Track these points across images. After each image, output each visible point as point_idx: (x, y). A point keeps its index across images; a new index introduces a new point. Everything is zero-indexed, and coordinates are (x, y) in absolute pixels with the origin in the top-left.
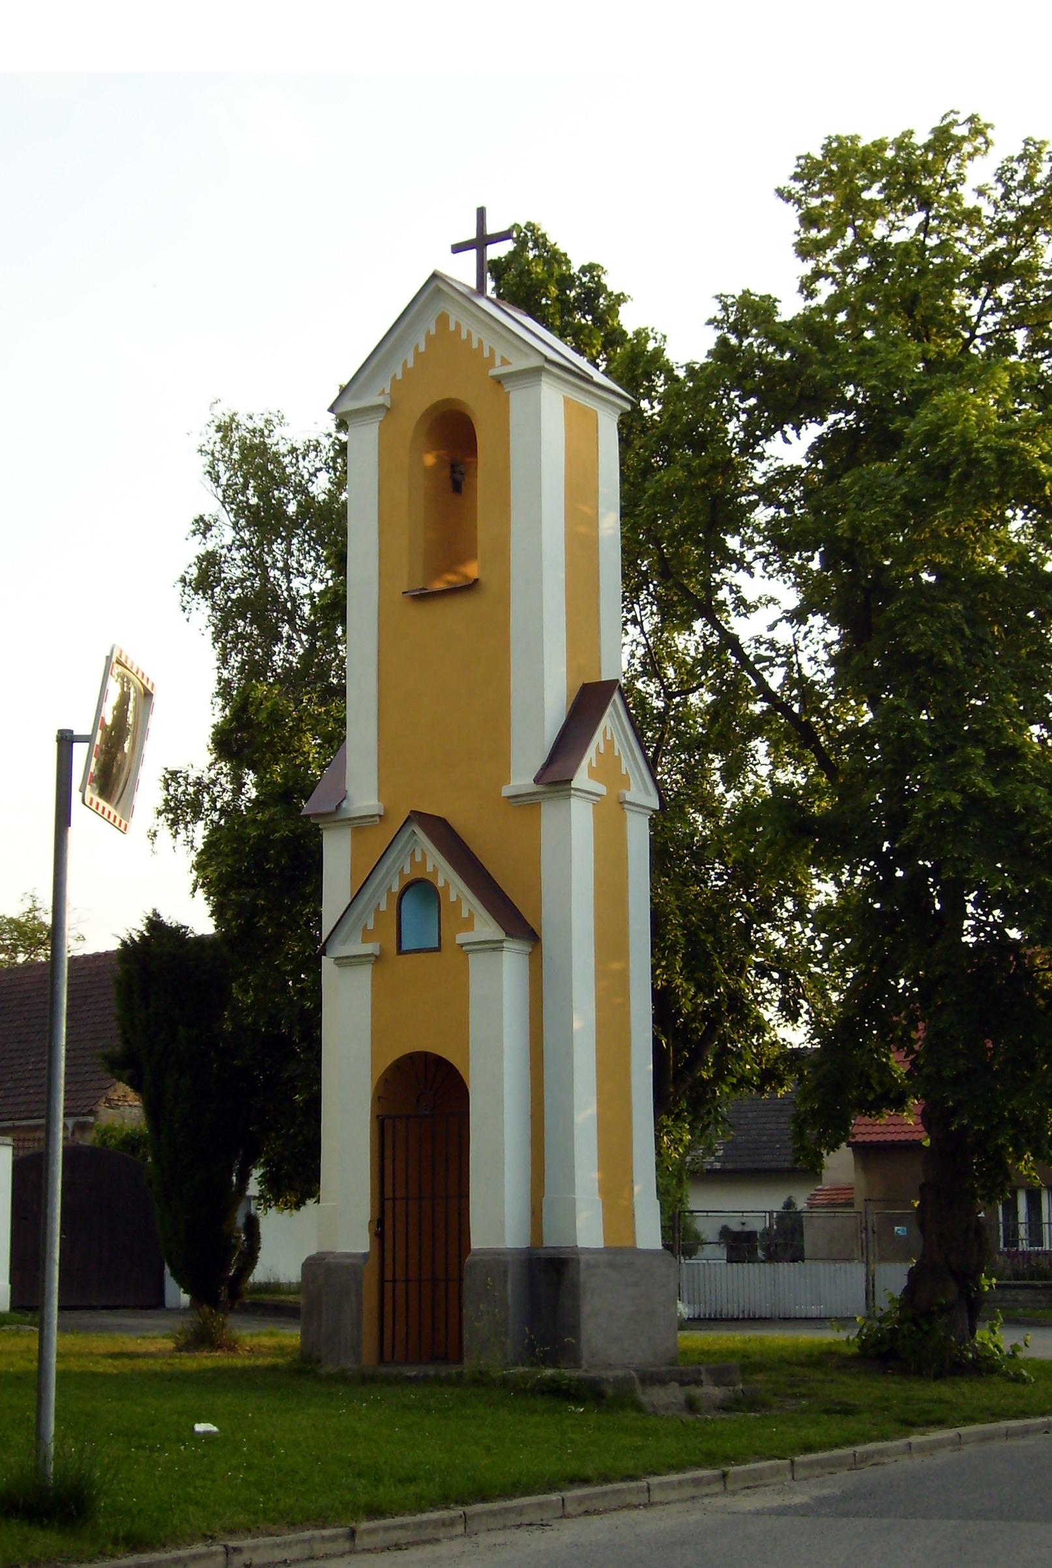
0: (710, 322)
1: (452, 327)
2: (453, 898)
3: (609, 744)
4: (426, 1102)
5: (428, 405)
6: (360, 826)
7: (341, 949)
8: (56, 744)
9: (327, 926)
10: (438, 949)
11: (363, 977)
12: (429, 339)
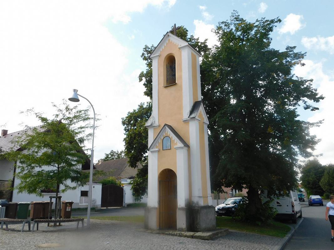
0: (217, 26)
1: (171, 41)
2: (173, 139)
3: (201, 112)
4: (168, 178)
5: (167, 54)
7: (151, 150)
10: (170, 149)
11: (156, 155)
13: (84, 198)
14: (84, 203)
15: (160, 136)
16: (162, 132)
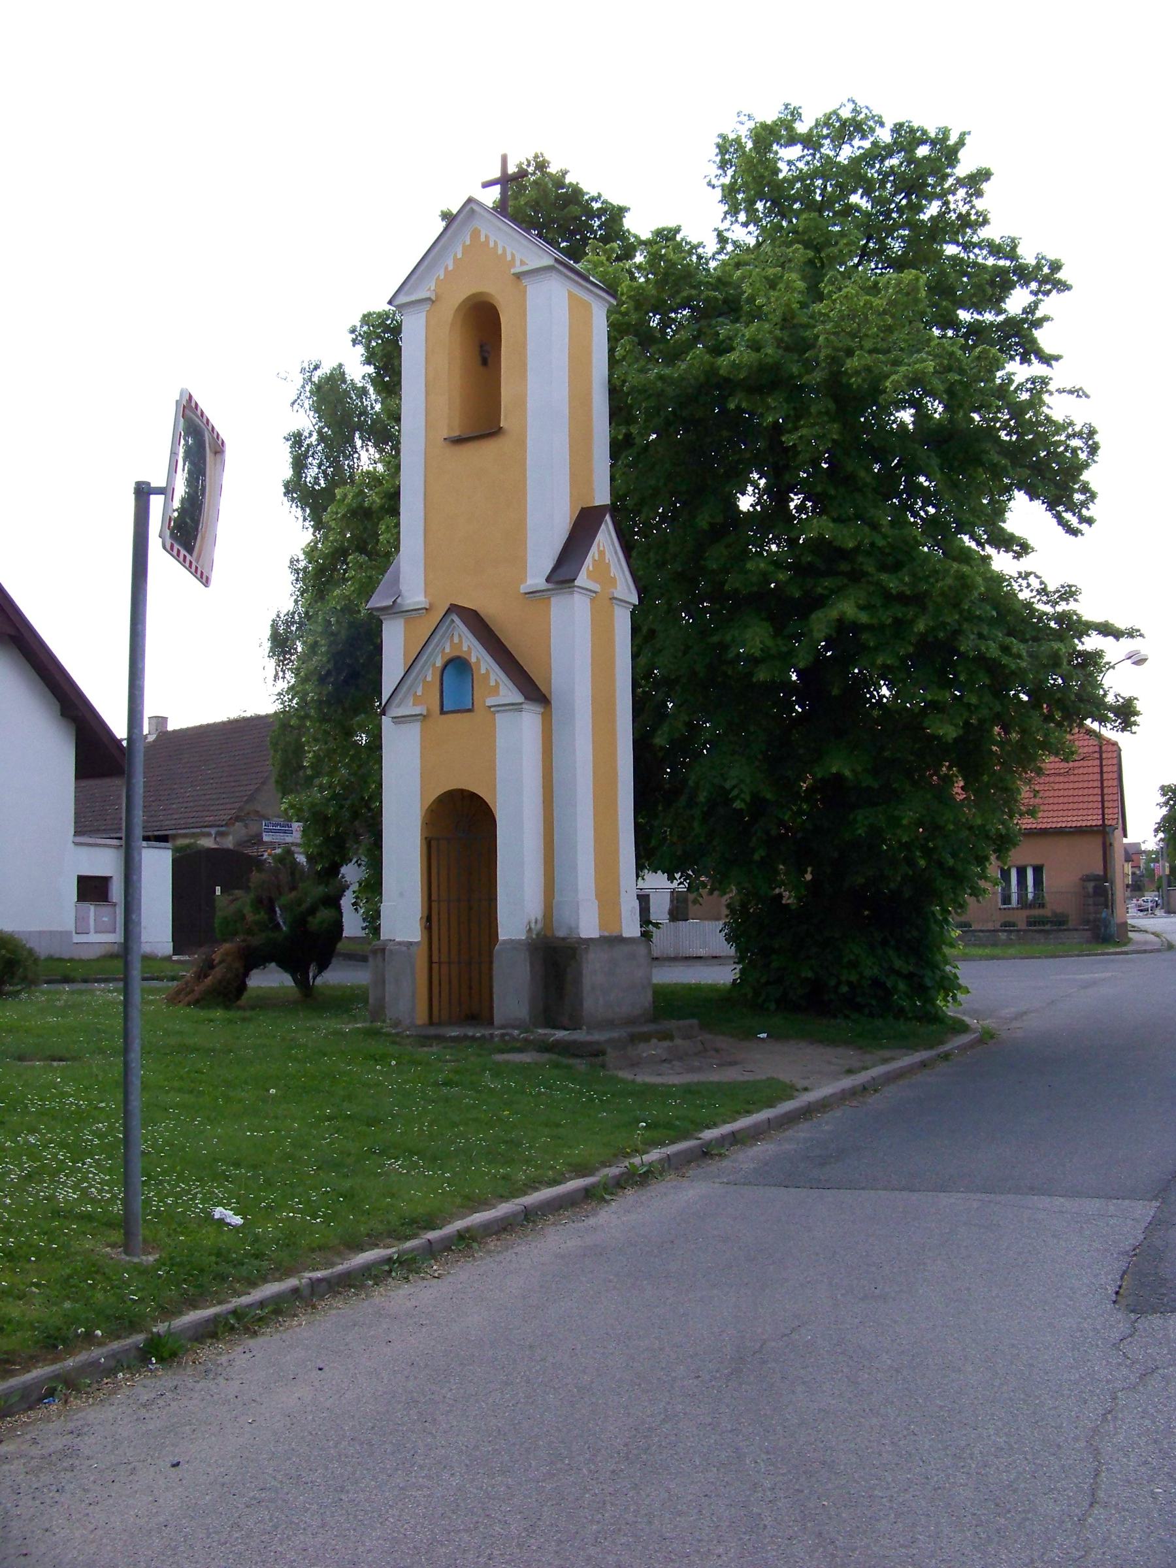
1: (483, 239)
2: (483, 671)
4: (463, 828)
6: (411, 615)
8: (133, 496)
9: (385, 696)
11: (413, 732)
12: (466, 250)
13: (91, 909)
14: (92, 930)
15: (423, 667)
16: (437, 637)
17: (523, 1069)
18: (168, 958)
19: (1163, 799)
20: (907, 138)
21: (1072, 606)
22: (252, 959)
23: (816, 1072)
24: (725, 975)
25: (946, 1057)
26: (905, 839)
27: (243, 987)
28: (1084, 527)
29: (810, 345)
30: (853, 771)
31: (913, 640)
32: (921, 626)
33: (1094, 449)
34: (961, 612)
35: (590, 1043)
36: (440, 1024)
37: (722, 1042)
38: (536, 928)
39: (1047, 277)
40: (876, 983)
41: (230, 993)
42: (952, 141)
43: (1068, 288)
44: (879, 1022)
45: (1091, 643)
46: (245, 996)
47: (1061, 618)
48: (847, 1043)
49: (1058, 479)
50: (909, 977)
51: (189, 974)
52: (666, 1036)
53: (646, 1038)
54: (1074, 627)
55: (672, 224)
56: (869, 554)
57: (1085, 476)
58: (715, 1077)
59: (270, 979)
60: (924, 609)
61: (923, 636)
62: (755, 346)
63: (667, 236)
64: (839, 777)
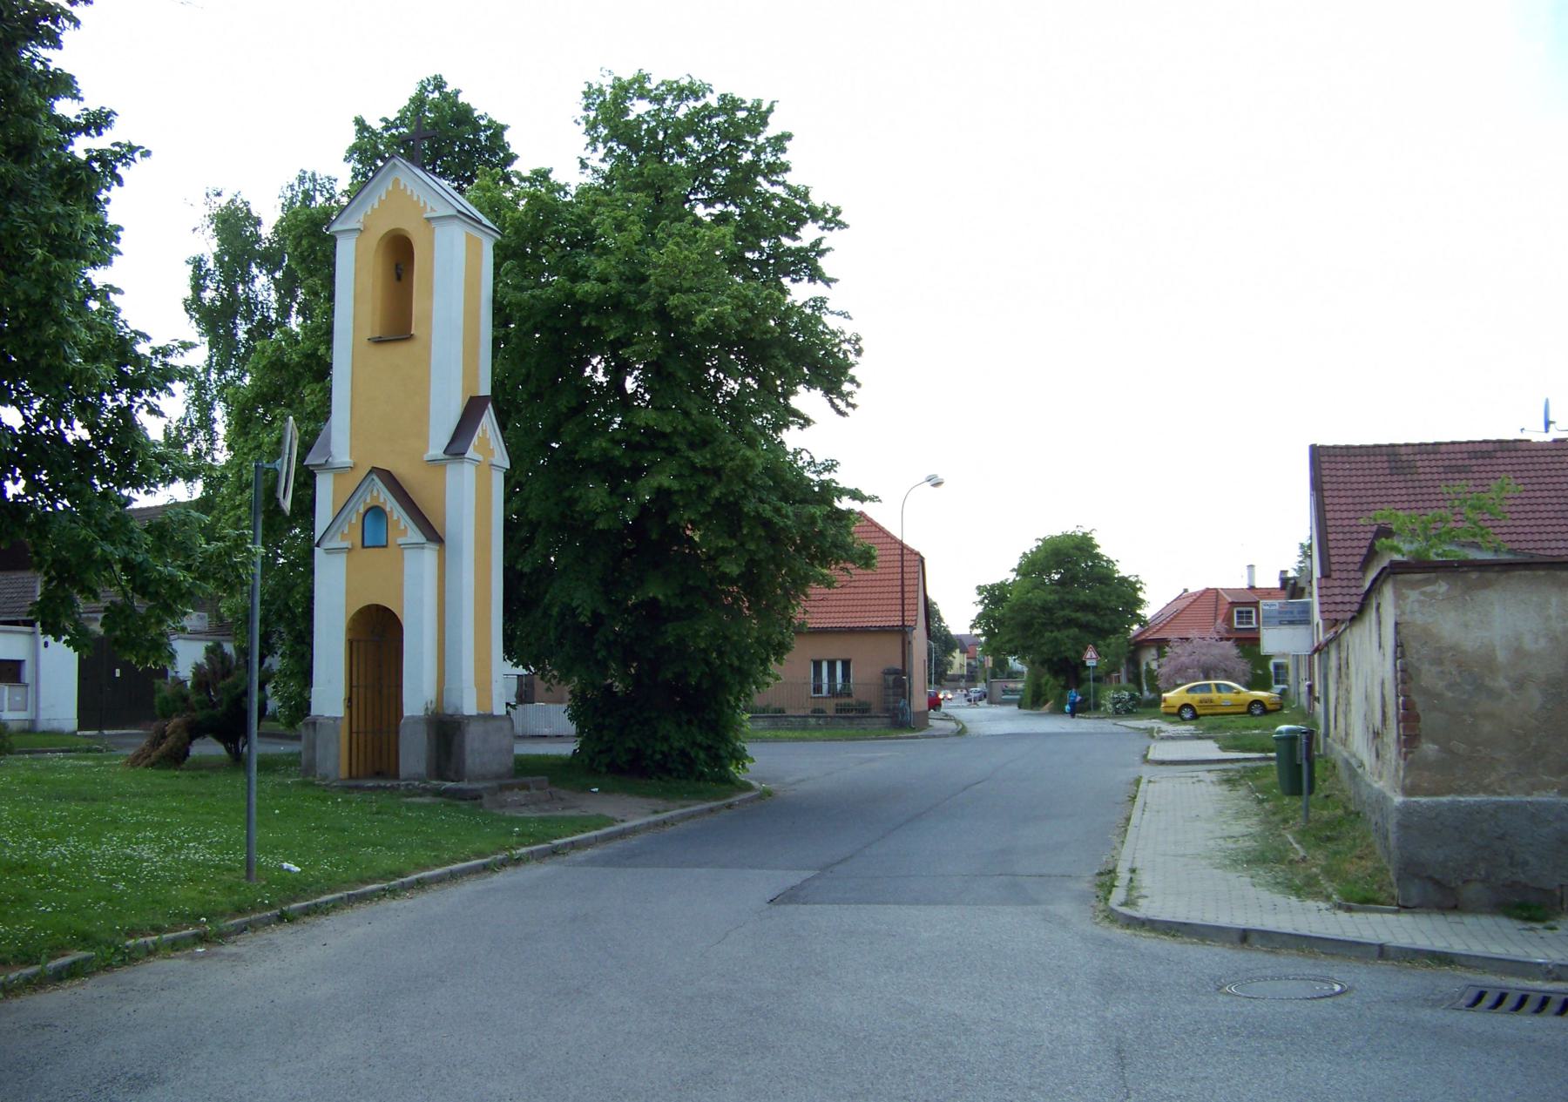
3: (484, 432)
4: (378, 632)
6: (340, 471)
7: (327, 544)
11: (340, 561)
12: (388, 193)
17: (421, 806)
18: (74, 733)
19: (979, 598)
20: (729, 105)
21: (832, 476)
22: (196, 731)
23: (633, 812)
24: (567, 749)
25: (730, 806)
26: (703, 646)
27: (187, 754)
28: (849, 410)
29: (644, 279)
30: (666, 596)
31: (711, 501)
32: (716, 493)
33: (859, 352)
34: (746, 482)
35: (472, 790)
36: (357, 778)
37: (563, 793)
38: (432, 707)
39: (832, 219)
40: (683, 753)
41: (177, 758)
42: (764, 108)
43: (846, 226)
44: (684, 782)
45: (844, 504)
46: (189, 760)
47: (822, 484)
48: (657, 796)
49: (831, 374)
50: (709, 748)
51: (144, 742)
52: (525, 787)
53: (510, 788)
54: (829, 492)
55: (547, 167)
56: (681, 435)
57: (851, 372)
58: (559, 813)
59: (208, 748)
60: (720, 479)
61: (718, 500)
62: (604, 280)
63: (542, 175)
64: (654, 600)
